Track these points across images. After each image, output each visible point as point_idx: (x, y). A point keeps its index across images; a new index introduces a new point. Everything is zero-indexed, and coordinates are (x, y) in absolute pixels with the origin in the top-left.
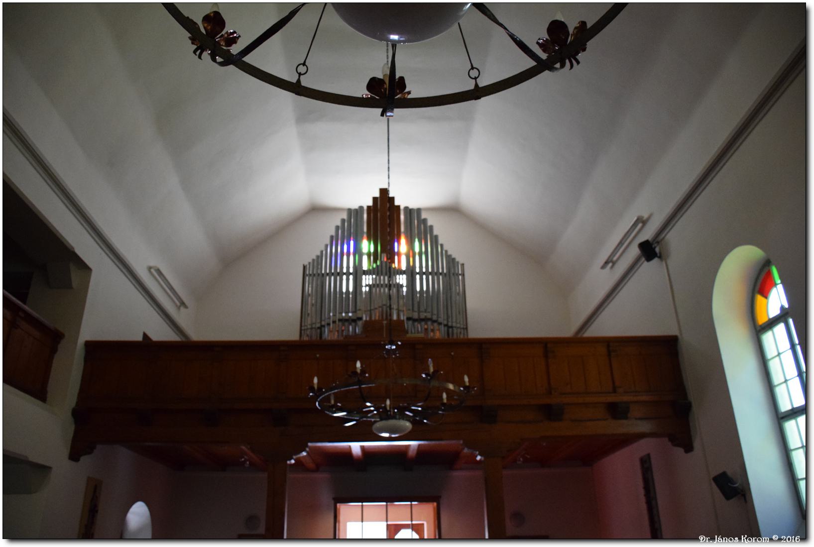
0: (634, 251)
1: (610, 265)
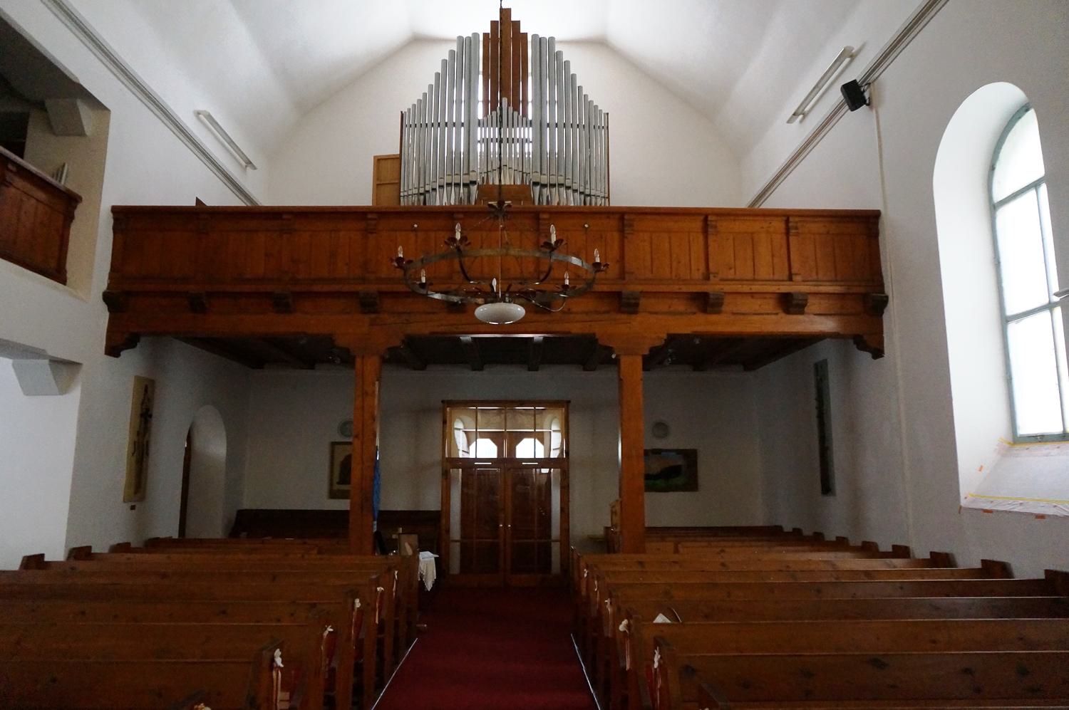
0: (836, 96)
1: (801, 116)
